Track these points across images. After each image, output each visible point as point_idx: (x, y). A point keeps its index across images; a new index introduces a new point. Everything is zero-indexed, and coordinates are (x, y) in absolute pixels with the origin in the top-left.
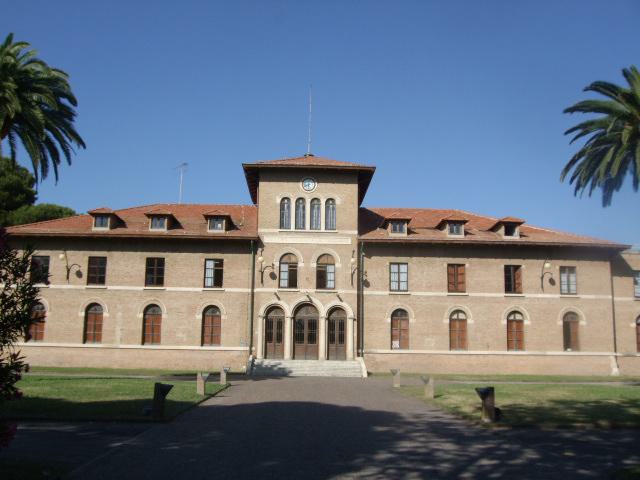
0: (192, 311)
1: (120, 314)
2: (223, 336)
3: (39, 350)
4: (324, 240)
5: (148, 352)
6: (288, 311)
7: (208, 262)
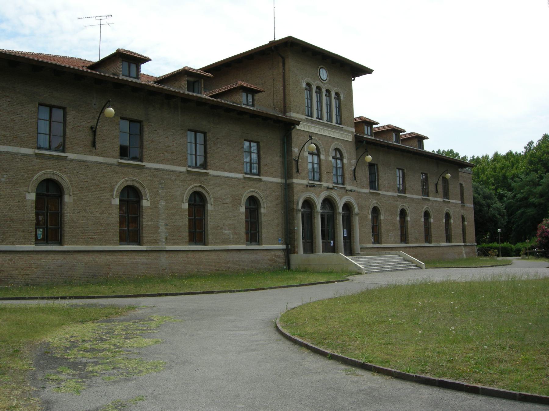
0: (236, 202)
1: (163, 203)
3: (59, 257)
5: (197, 255)
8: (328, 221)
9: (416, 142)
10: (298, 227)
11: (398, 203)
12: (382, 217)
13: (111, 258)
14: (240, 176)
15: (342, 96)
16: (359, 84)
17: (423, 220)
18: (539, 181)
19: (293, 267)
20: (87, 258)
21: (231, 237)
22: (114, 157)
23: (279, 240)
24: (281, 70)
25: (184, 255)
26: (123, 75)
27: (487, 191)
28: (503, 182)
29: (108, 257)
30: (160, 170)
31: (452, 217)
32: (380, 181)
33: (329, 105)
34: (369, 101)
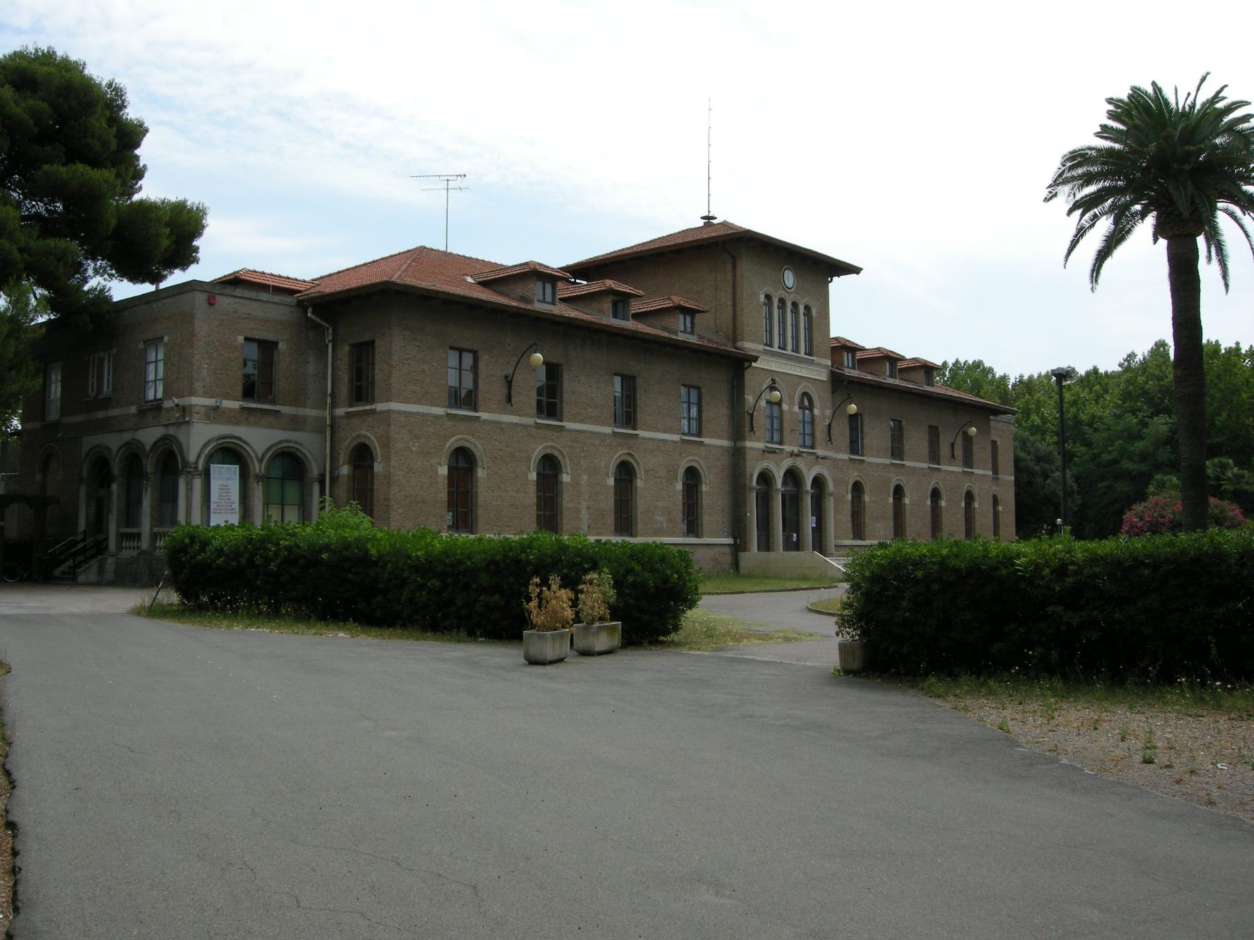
1: (585, 477)
8: (792, 502)
9: (921, 376)
10: (751, 512)
11: (892, 475)
12: (867, 498)
14: (676, 437)
15: (814, 311)
16: (838, 286)
17: (929, 503)
18: (1139, 431)
19: (742, 571)
22: (529, 416)
24: (730, 275)
25: (706, 549)
27: (1043, 447)
28: (1070, 429)
30: (582, 432)
31: (977, 498)
32: (866, 441)
33: (796, 326)
34: (854, 315)
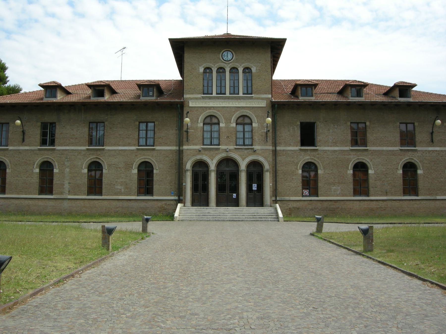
2: (156, 187)
4: (211, 104)
5: (92, 202)
6: (213, 166)
7: (141, 124)
13: (30, 202)
20: (17, 202)
21: (123, 190)
23: (172, 193)
26: (352, 97)
29: (29, 202)
30: (66, 150)
